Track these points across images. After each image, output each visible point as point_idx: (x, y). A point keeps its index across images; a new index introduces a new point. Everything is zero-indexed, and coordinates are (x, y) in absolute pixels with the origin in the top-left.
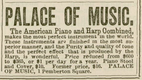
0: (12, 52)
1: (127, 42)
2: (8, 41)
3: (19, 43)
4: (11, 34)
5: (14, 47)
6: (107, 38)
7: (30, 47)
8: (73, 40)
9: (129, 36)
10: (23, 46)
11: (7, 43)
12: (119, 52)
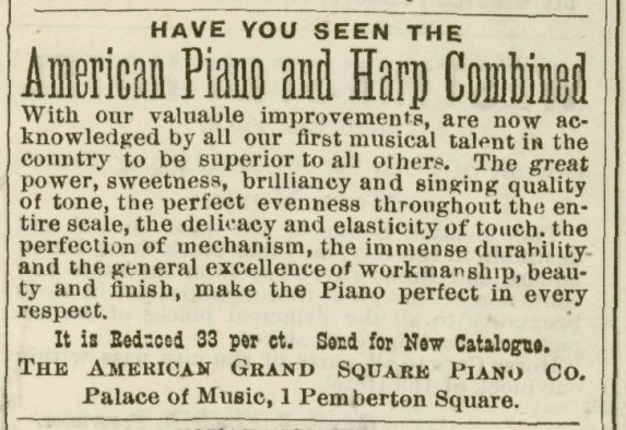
1: (346, 206)
2: (486, 158)
4: (183, 97)
5: (266, 159)
6: (377, 210)
8: (314, 128)
9: (273, 159)
11: (482, 168)
12: (184, 142)
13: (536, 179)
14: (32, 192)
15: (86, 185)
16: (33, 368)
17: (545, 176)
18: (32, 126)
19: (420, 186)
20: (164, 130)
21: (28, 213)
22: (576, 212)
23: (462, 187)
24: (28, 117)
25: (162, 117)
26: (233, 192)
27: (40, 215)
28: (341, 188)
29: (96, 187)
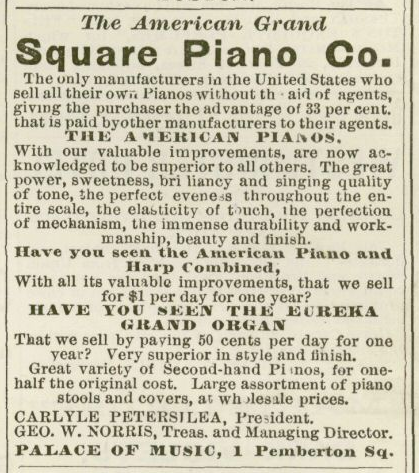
0: (263, 182)
3: (225, 227)
7: (119, 78)
10: (167, 122)
13: (357, 177)
14: (22, 187)
15: (57, 183)
16: (24, 340)
17: (363, 175)
18: (22, 159)
19: (279, 183)
20: (109, 161)
21: (19, 202)
22: (384, 200)
23: (306, 183)
24: (19, 153)
25: (106, 152)
26: (155, 189)
27: (26, 203)
28: (225, 185)
29: (64, 184)
